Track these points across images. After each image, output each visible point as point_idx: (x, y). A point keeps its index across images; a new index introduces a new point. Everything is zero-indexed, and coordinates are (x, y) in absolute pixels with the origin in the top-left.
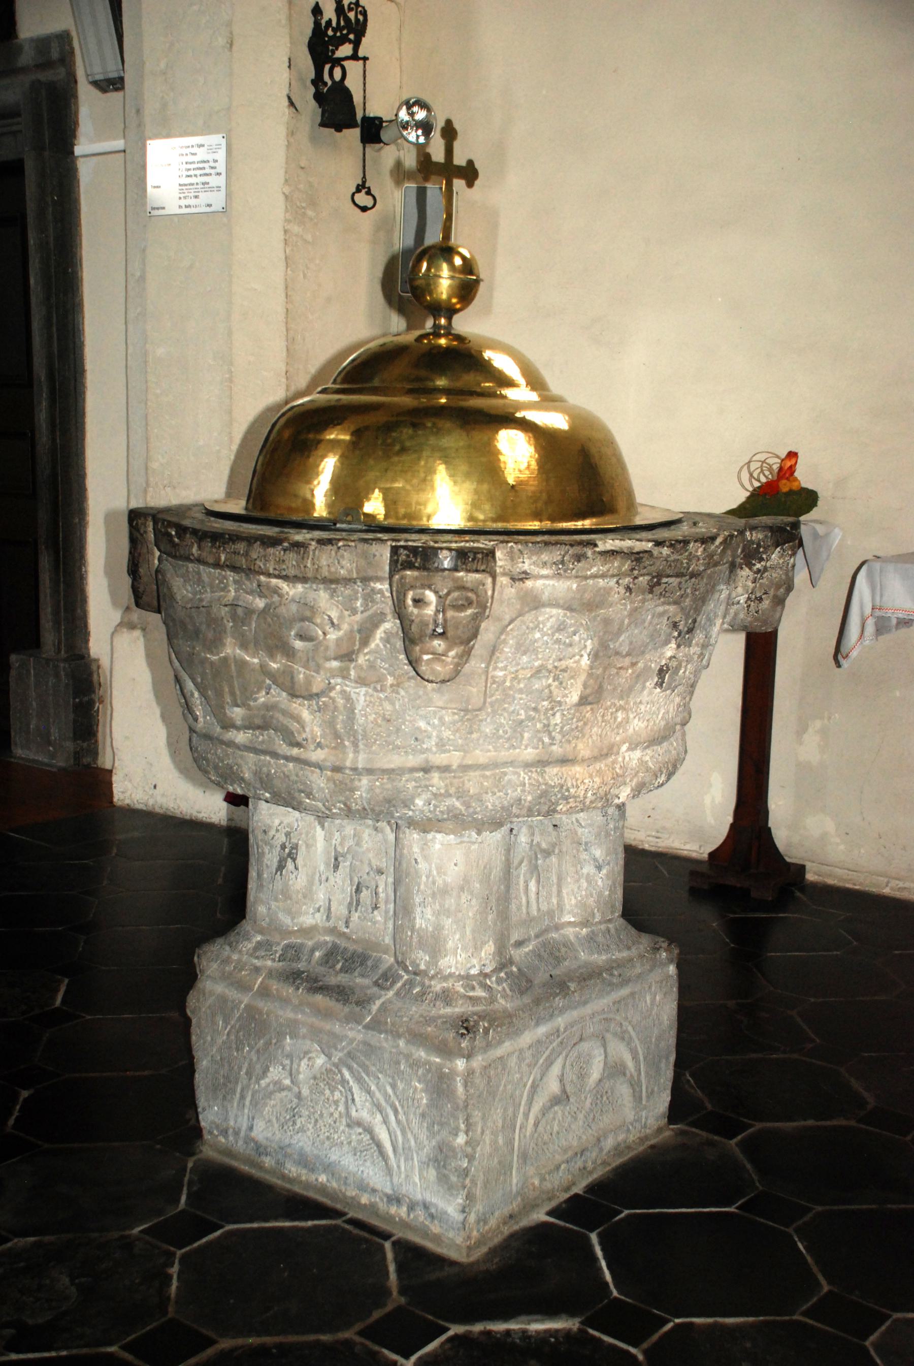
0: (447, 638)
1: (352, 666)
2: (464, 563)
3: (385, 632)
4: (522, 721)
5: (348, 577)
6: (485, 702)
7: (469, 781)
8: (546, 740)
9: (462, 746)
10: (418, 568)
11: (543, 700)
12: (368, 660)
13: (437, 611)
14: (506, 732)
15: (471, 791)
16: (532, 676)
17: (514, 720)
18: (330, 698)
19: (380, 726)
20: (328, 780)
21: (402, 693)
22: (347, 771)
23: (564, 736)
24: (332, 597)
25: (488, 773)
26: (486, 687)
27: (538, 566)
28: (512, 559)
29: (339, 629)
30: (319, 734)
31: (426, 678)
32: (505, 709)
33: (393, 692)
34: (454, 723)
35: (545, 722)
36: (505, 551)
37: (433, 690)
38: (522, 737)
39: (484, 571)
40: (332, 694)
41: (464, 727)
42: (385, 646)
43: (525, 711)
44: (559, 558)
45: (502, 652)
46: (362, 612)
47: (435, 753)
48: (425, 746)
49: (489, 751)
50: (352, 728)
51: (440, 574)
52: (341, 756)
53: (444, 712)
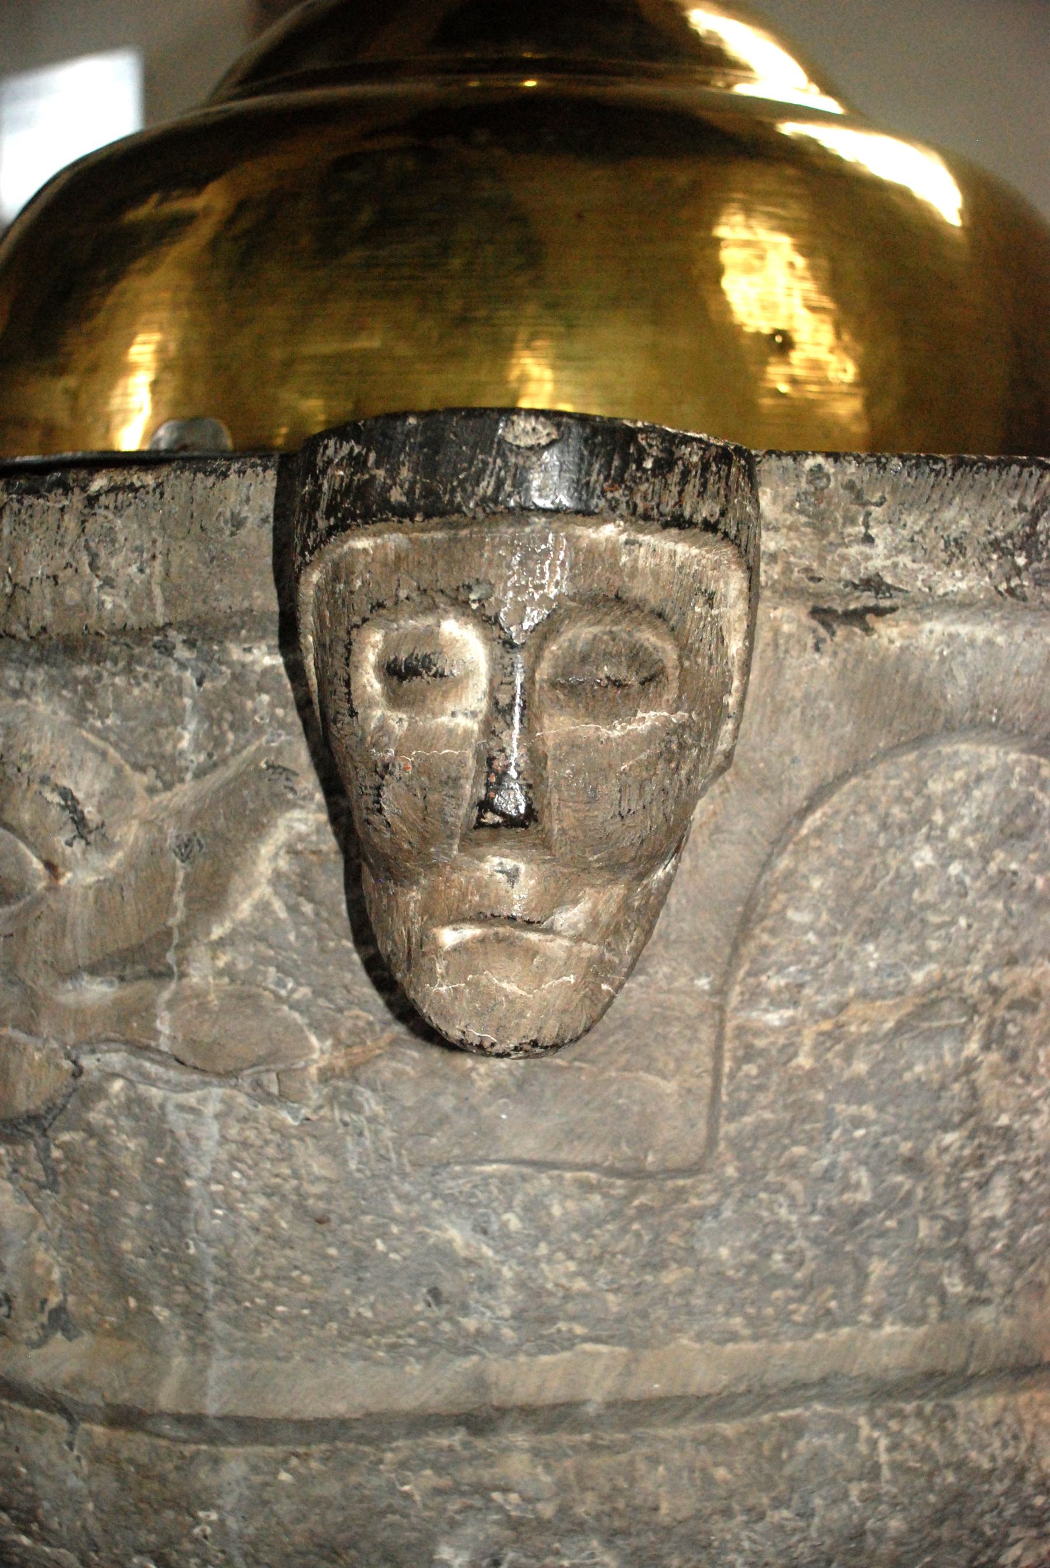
0: (546, 844)
1: (166, 995)
2: (619, 480)
3: (292, 851)
4: (862, 1212)
5: (133, 621)
6: (712, 1142)
7: (654, 1461)
8: (955, 1285)
9: (620, 1319)
10: (404, 513)
11: (946, 1127)
12: (228, 971)
13: (499, 711)
14: (795, 1259)
15: (665, 1508)
16: (900, 1028)
17: (829, 1211)
18: (90, 1131)
19: (288, 1243)
20: (97, 1458)
21: (371, 1103)
22: (166, 1428)
23: (1020, 1269)
24: (80, 715)
25: (728, 1428)
26: (716, 1073)
27: (928, 557)
28: (820, 524)
29: (107, 846)
30: (56, 1275)
31: (455, 1033)
32: (792, 1165)
33: (332, 1100)
34: (586, 1225)
35: (950, 1212)
36: (789, 491)
37: (498, 1090)
38: (863, 1275)
39: (710, 527)
40: (96, 1116)
41: (628, 1241)
42: (293, 909)
43: (876, 1174)
44: (1016, 522)
45: (781, 926)
46: (200, 773)
47: (513, 1351)
48: (471, 1324)
49: (733, 1337)
50: (177, 1256)
51: (506, 531)
52: (139, 1362)
53: (545, 1180)
